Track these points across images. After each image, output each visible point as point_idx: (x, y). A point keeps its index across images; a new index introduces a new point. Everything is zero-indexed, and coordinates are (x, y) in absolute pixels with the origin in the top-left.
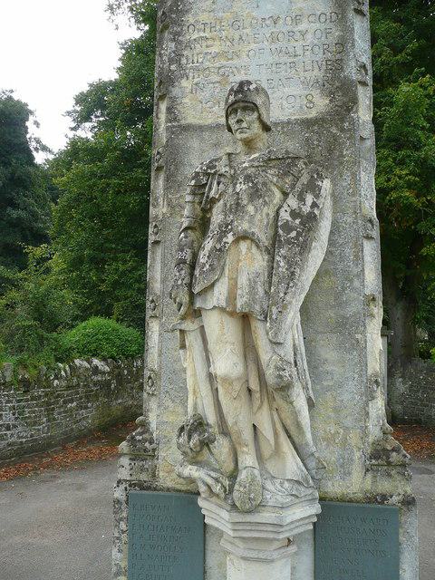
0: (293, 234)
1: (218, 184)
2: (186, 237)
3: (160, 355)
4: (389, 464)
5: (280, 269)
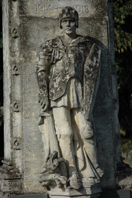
0: (90, 75)
1: (59, 52)
2: (42, 75)
3: (22, 130)
4: (125, 172)
5: (87, 90)
